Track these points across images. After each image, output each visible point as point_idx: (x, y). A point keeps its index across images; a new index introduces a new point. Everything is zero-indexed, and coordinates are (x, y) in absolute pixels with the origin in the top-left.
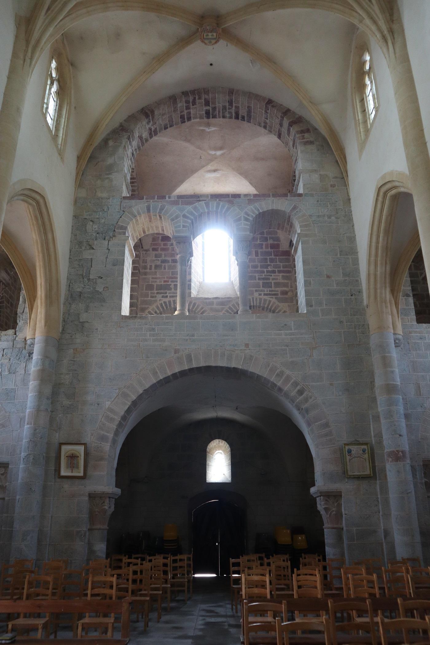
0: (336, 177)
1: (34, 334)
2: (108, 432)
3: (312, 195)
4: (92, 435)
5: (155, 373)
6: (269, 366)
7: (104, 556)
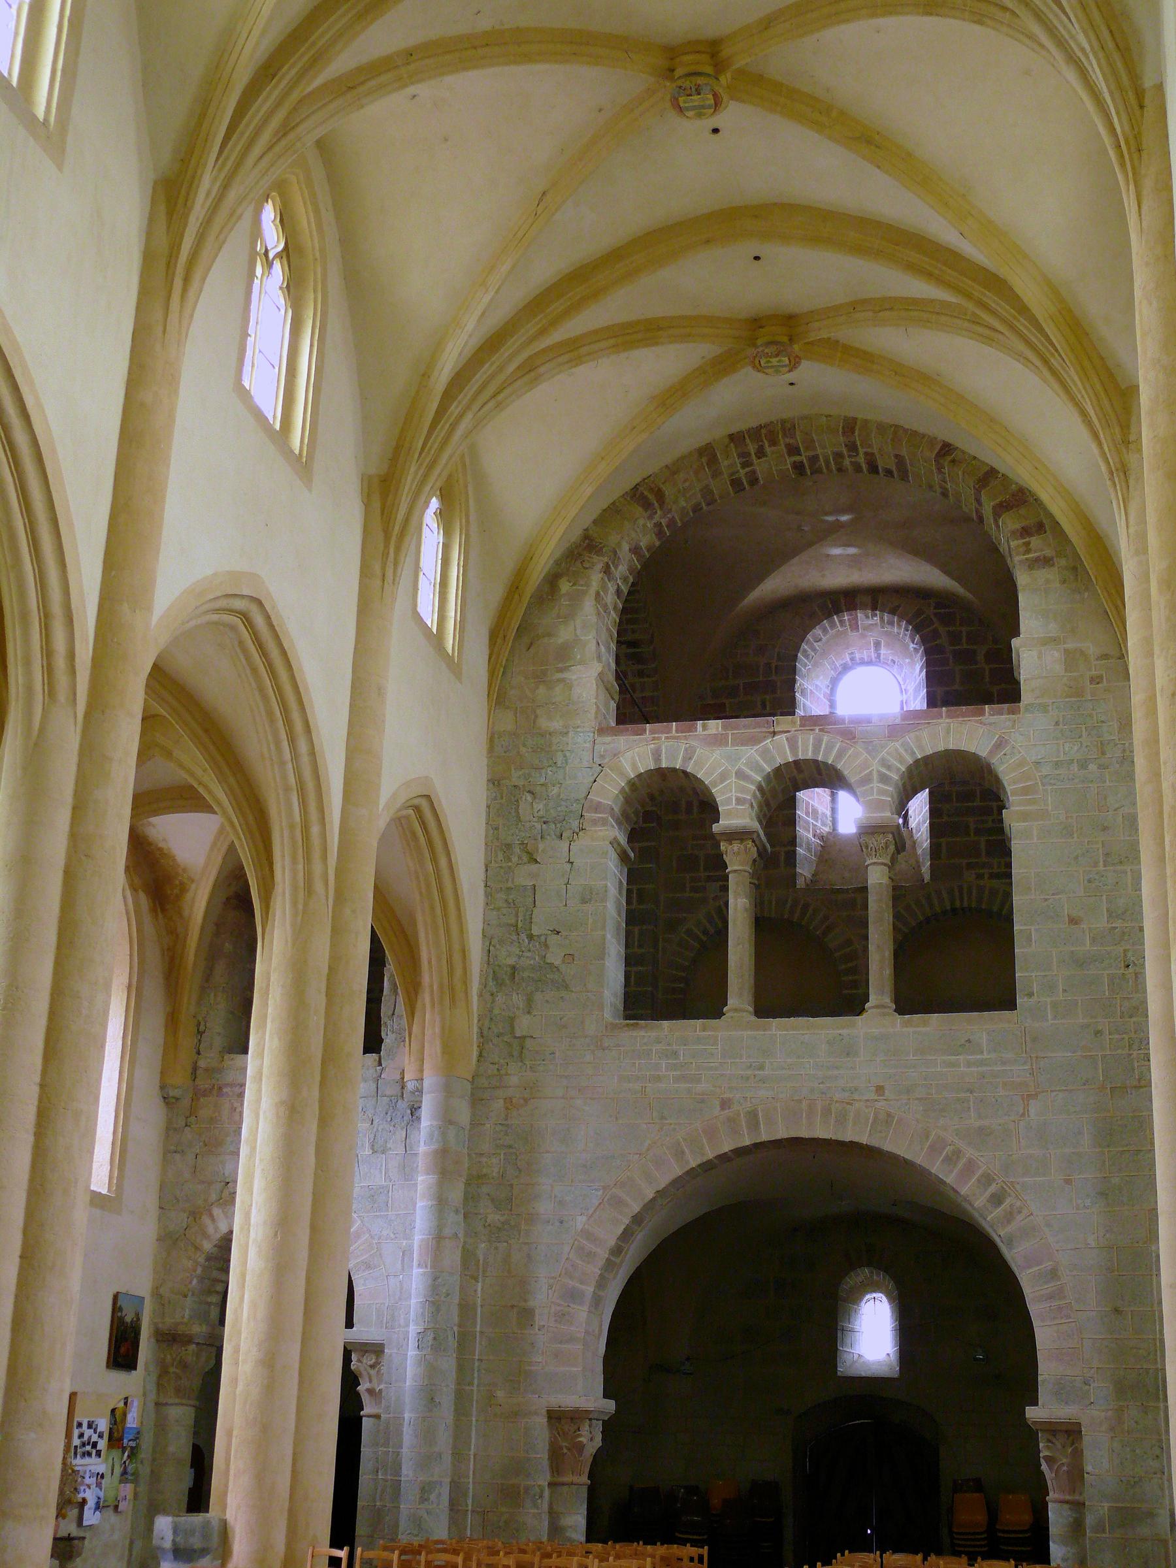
0: (1105, 656)
1: (422, 1071)
2: (582, 1283)
3: (1044, 708)
4: (550, 1287)
5: (679, 1154)
6: (927, 1137)
7: (583, 1539)
